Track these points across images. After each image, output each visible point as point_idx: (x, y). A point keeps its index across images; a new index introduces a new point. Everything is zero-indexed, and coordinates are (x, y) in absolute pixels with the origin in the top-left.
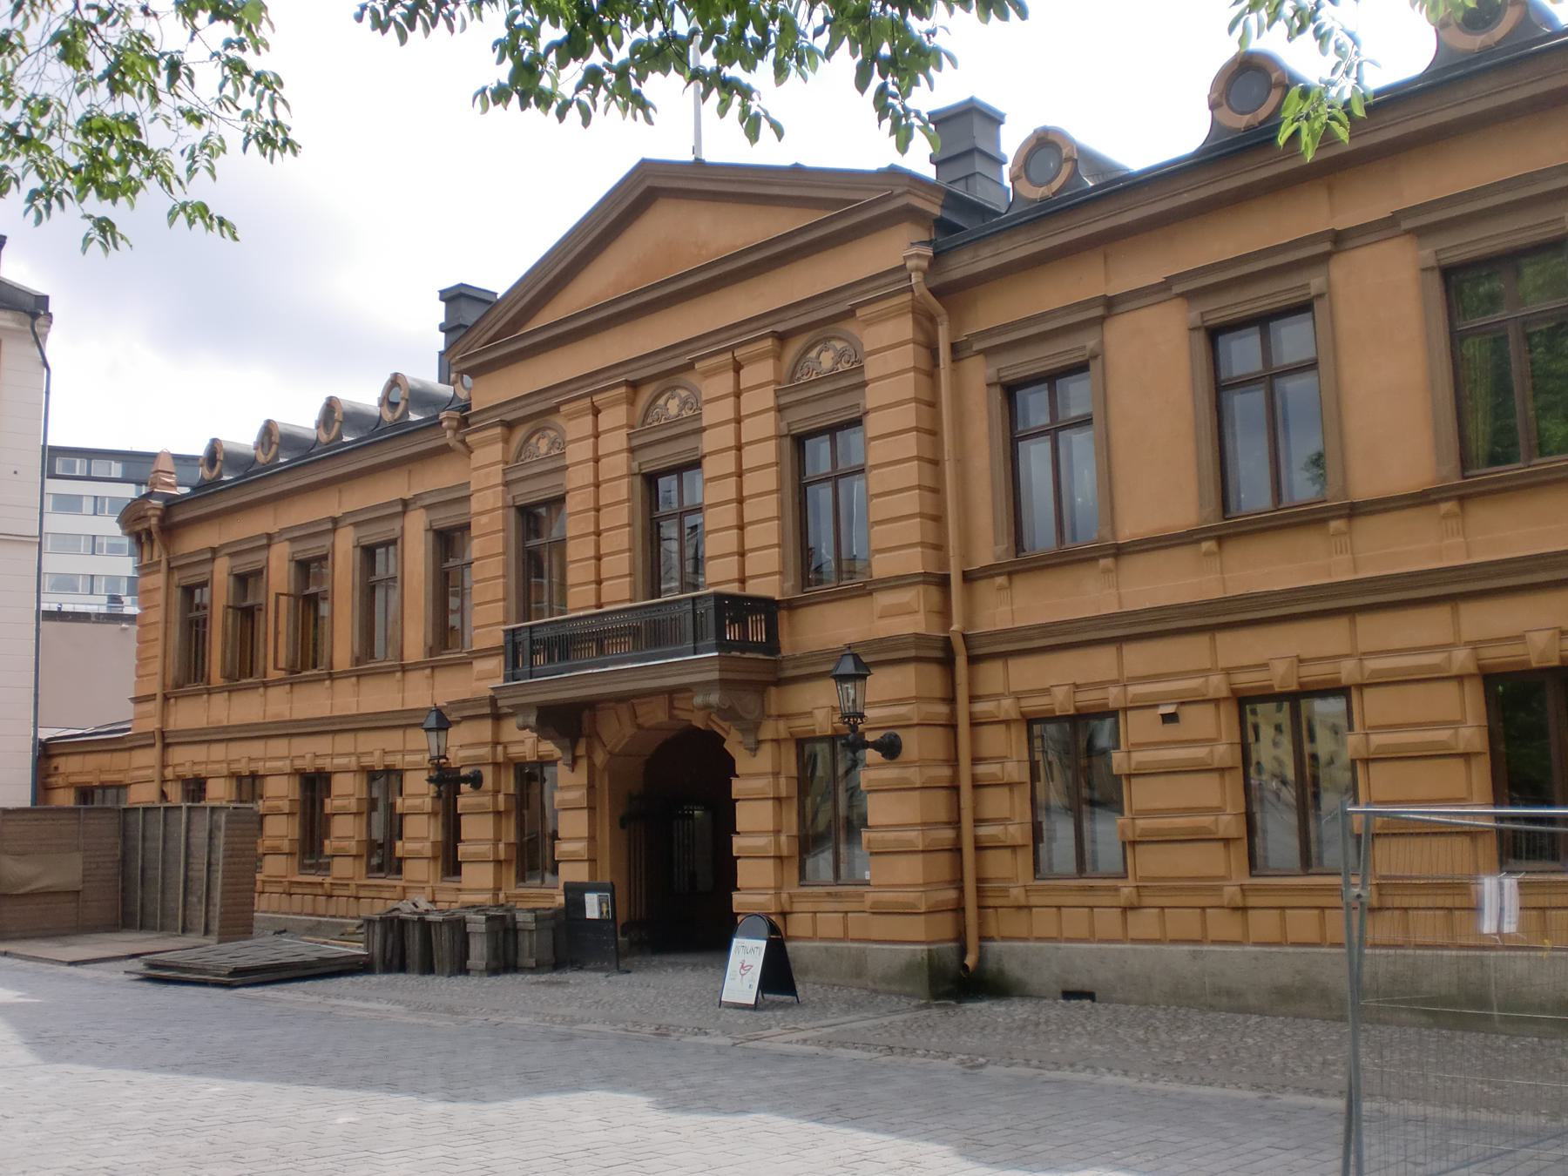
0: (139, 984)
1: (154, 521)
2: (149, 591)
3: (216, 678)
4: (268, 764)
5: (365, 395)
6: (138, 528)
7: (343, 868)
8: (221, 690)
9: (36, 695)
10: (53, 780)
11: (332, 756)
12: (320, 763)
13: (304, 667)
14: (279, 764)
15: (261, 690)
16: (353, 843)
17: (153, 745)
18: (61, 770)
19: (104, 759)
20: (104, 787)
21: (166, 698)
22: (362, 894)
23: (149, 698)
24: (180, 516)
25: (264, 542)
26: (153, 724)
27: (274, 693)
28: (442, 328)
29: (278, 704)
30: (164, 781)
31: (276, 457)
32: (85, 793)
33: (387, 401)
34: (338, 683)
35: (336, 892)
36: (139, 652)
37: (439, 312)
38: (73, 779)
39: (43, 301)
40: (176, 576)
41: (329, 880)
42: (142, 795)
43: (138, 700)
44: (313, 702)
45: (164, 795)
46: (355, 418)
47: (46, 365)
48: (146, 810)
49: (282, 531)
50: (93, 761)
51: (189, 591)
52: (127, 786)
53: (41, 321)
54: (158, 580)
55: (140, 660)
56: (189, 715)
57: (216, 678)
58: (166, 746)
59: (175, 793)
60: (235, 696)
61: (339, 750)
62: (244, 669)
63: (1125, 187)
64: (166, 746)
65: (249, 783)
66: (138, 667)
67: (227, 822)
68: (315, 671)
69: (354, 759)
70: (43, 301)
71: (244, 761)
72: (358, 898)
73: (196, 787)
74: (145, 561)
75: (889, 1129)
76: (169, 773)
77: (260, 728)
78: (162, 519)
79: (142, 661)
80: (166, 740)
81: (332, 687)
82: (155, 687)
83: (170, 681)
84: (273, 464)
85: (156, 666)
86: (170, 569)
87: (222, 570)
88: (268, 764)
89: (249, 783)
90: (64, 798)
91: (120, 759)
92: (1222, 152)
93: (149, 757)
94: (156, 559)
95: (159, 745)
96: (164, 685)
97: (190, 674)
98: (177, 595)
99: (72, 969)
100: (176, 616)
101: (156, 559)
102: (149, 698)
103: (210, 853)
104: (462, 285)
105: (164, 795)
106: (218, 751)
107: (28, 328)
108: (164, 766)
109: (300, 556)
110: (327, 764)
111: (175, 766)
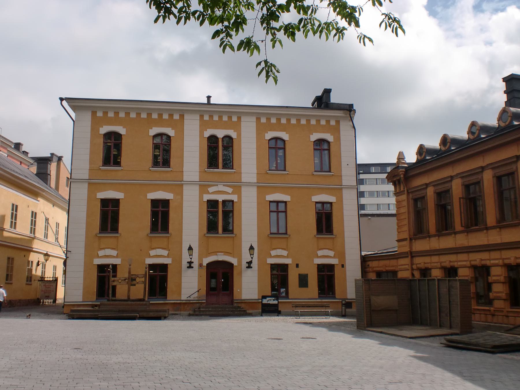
0: (446, 348)
1: (402, 176)
2: (400, 201)
3: (458, 227)
4: (459, 263)
5: (434, 143)
6: (395, 179)
7: (498, 304)
8: (435, 236)
9: (360, 240)
10: (368, 269)
11: (490, 260)
12: (426, 265)
13: (472, 226)
14: (497, 262)
15: (453, 235)
16: (504, 294)
17: (407, 257)
18: (370, 266)
19: (387, 262)
20: (387, 272)
21: (411, 239)
22: (509, 315)
23: (405, 240)
24: (411, 173)
25: (450, 179)
26: (406, 249)
27: (458, 236)
28: (505, 92)
29: (435, 243)
30: (413, 269)
31: (450, 147)
32: (379, 274)
33: (470, 132)
34: (490, 231)
35: (496, 314)
36: (398, 224)
37: (503, 86)
38: (375, 269)
39: (351, 106)
40: (411, 195)
41: (492, 309)
42: (404, 274)
43: (398, 241)
44: (478, 239)
45: (413, 275)
46: (431, 151)
47: (354, 127)
48: (438, 280)
49: (457, 175)
50: (382, 263)
51: (416, 200)
52: (430, 269)
53: (352, 112)
54: (404, 197)
55: (398, 226)
56: (420, 245)
57: (458, 227)
58: (412, 257)
59: (417, 275)
60: (441, 238)
61: (492, 257)
62: (445, 226)
63: (414, 164)
64: (412, 257)
65: (482, 271)
66: (398, 229)
67: (460, 286)
68: (477, 227)
69: (439, 264)
70: (351, 106)
71: (448, 262)
72: (507, 316)
73: (425, 272)
74: (398, 191)
75: (371, 339)
76: (414, 267)
77: (443, 250)
78: (404, 175)
79: (399, 227)
80: (412, 255)
81: (487, 233)
82: (406, 235)
83: (412, 234)
84: (449, 150)
85: (406, 228)
86: (408, 193)
87: (430, 192)
88: (459, 263)
89: (482, 271)
90: (372, 276)
91: (393, 262)
92: (418, 161)
93: (405, 261)
94: (402, 189)
95: (409, 257)
96: (410, 235)
97: (419, 230)
98: (411, 202)
99: (411, 340)
100: (412, 210)
101: (402, 189)
102: (405, 240)
103: (449, 297)
104: (512, 75)
105: (413, 275)
106: (435, 259)
107: (348, 115)
108: (412, 264)
109: (437, 191)
110: (429, 266)
111: (416, 264)
